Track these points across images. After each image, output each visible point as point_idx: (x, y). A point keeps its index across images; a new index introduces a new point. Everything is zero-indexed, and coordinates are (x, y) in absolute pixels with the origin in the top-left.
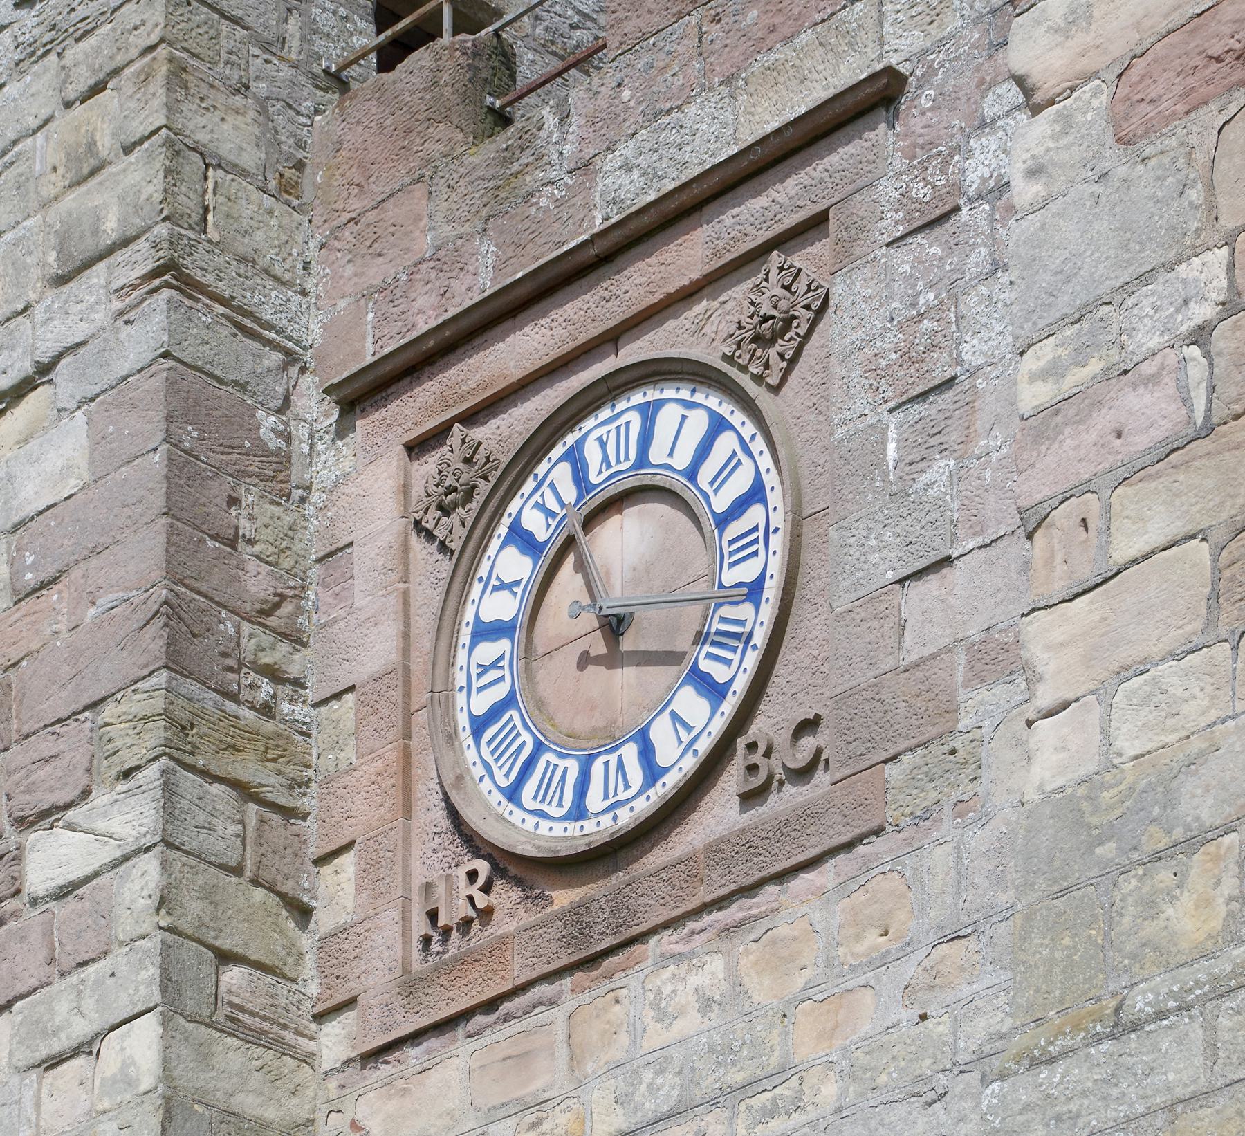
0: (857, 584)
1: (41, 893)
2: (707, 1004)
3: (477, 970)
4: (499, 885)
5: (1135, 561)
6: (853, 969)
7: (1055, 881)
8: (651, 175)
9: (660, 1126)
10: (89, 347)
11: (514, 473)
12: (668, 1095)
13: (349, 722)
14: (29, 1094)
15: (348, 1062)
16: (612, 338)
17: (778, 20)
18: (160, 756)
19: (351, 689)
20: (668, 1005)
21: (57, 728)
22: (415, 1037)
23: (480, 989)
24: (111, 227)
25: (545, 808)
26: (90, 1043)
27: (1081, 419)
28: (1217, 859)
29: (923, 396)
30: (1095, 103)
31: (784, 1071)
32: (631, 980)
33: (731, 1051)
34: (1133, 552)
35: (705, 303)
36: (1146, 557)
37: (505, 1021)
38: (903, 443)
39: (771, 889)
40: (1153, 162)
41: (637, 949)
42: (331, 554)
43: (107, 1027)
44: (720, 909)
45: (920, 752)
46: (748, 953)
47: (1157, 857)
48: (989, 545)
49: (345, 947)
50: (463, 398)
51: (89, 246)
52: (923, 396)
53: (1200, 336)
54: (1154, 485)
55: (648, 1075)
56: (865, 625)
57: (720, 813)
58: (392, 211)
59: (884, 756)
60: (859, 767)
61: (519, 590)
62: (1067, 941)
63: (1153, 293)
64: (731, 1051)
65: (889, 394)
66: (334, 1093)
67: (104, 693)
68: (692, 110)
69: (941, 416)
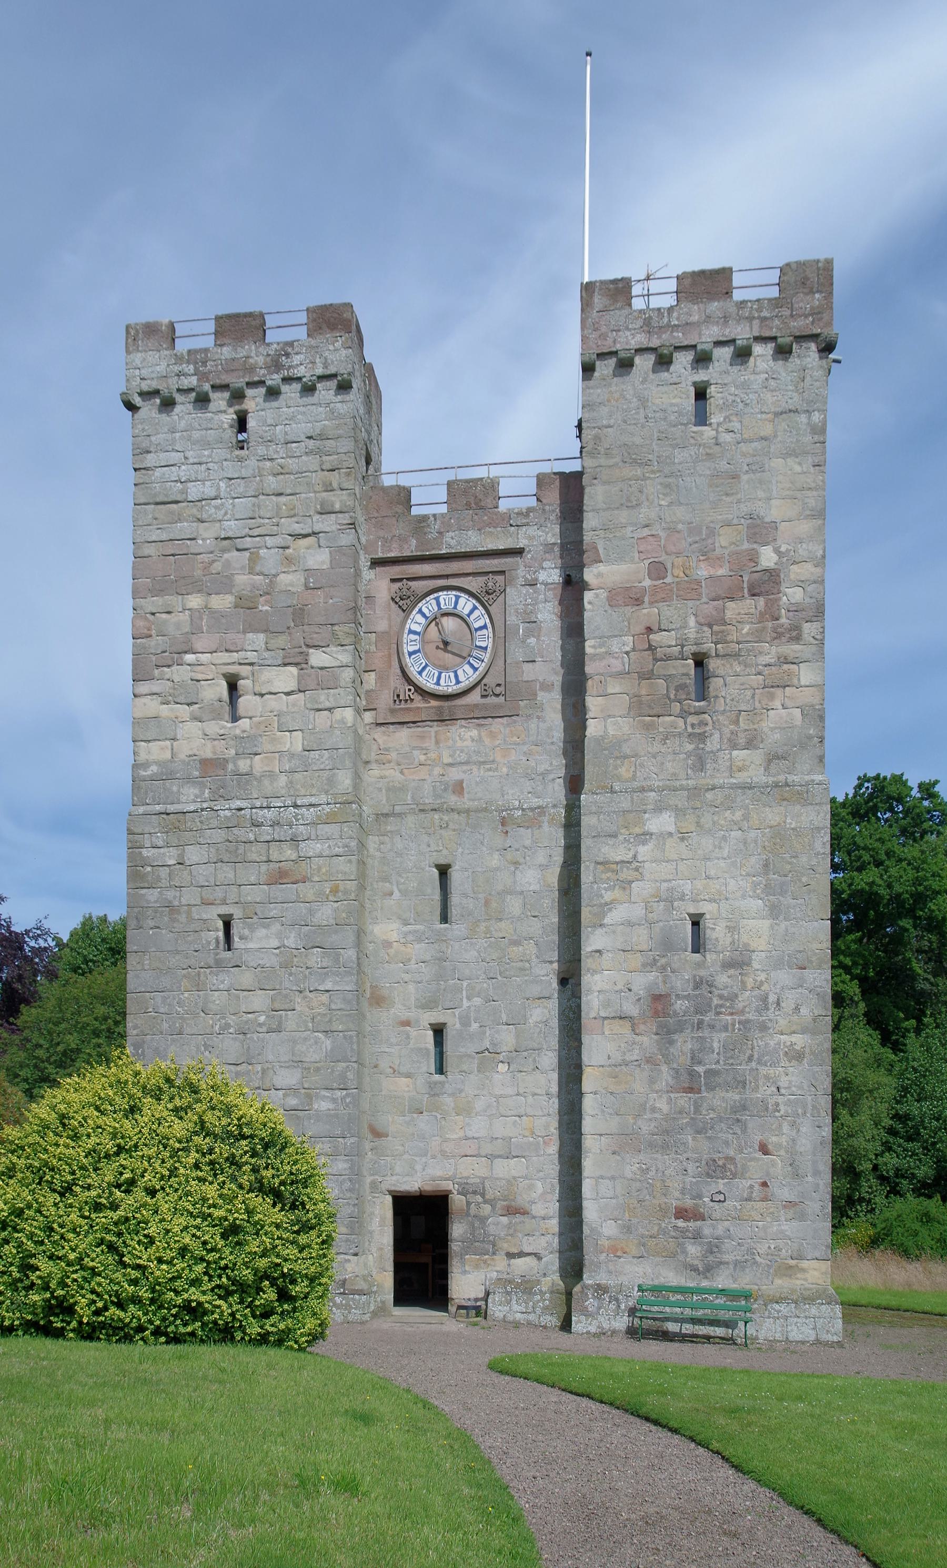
1: (315, 666)
3: (412, 713)
8: (459, 543)
13: (374, 640)
14: (311, 717)
16: (447, 577)
22: (393, 724)
24: (337, 507)
27: (601, 660)
32: (453, 728)
47: (617, 758)
51: (330, 509)
53: (627, 653)
55: (458, 752)
57: (475, 697)
58: (386, 520)
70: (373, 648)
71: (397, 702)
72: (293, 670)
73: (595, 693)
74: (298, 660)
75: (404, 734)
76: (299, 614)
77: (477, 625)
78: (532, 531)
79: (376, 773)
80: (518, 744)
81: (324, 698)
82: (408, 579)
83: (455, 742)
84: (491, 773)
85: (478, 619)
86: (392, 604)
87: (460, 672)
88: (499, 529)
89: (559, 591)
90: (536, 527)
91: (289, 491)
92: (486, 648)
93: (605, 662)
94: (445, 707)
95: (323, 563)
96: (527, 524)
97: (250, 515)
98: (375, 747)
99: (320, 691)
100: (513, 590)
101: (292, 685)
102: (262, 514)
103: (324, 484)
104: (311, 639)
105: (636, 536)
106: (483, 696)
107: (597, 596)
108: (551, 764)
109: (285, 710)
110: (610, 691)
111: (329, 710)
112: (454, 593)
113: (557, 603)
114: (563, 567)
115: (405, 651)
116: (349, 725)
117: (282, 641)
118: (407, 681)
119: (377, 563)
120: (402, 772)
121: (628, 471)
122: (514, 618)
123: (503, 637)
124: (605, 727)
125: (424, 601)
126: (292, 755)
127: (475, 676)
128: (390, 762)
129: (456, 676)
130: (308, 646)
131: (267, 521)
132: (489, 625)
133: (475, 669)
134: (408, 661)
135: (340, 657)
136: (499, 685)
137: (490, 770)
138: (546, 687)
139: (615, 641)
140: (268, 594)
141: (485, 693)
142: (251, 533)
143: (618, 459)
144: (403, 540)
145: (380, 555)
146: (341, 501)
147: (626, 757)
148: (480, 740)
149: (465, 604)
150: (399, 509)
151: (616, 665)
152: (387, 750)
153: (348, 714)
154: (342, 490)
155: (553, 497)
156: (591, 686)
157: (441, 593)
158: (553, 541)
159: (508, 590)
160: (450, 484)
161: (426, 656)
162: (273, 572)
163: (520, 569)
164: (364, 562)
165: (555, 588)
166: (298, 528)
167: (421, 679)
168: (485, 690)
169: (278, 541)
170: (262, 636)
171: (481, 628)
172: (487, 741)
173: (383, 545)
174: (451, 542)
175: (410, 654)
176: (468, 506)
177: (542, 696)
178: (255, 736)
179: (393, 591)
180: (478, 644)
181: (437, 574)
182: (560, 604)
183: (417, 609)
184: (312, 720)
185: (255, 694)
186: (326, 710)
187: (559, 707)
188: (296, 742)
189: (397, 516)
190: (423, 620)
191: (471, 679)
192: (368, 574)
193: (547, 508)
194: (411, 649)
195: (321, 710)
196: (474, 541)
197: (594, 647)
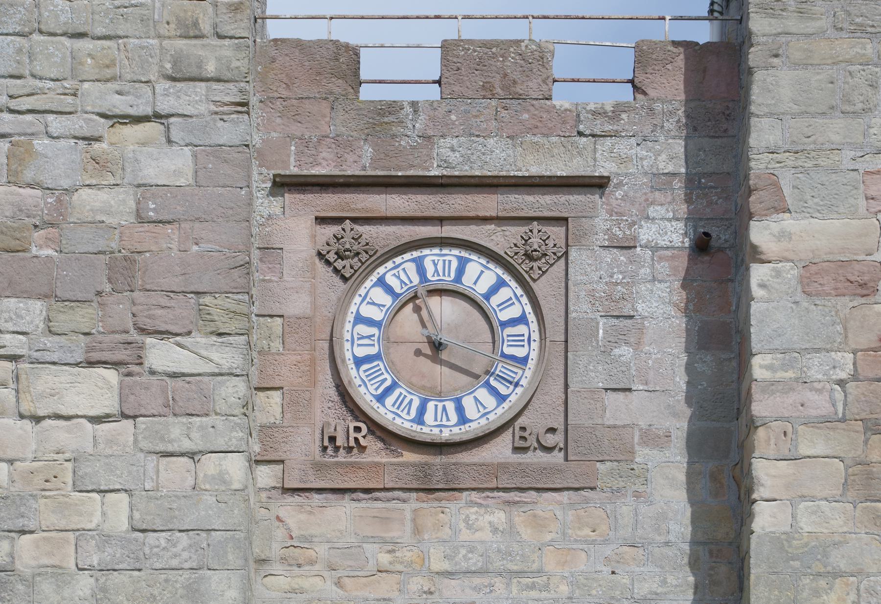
0: (582, 381)
1: (160, 369)
2: (495, 530)
3: (361, 473)
4: (370, 437)
5: (809, 457)
6: (576, 541)
7: (770, 567)
8: (467, 160)
9: (468, 575)
10: (190, 120)
12: (475, 564)
15: (274, 488)
16: (441, 220)
17: (539, 124)
20: (473, 524)
21: (172, 295)
22: (320, 491)
24: (211, 69)
25: (399, 412)
26: (194, 453)
28: (847, 585)
29: (618, 317)
30: (792, 272)
31: (540, 572)
32: (452, 507)
33: (510, 555)
34: (809, 453)
35: (493, 226)
36: (814, 457)
38: (605, 332)
39: (533, 493)
40: (820, 307)
41: (457, 494)
42: (267, 248)
45: (616, 463)
46: (519, 516)
47: (819, 574)
49: (276, 435)
50: (353, 210)
51: (194, 72)
52: (618, 317)
53: (841, 383)
54: (819, 431)
55: (463, 551)
56: (586, 401)
57: (500, 450)
58: (307, 105)
59: (597, 459)
60: (583, 458)
61: (385, 310)
62: (776, 593)
63: (819, 358)
64: (510, 555)
65: (600, 309)
66: (264, 499)
67: (205, 290)
68: (491, 141)
69: (625, 329)
70: (277, 345)
71: (330, 451)
72: (111, 376)
73: (772, 453)
74: (121, 355)
75: (344, 511)
76: (124, 269)
77: (504, 316)
78: (624, 147)
79: (282, 582)
80: (593, 542)
81: (178, 433)
82: (354, 220)
83: (456, 532)
84: (534, 594)
85: (507, 304)
86: (320, 265)
87: (468, 402)
88: (554, 139)
89: (683, 262)
90: (633, 141)
91: (100, 31)
92: (524, 361)
93: (792, 398)
94: (436, 465)
95: (177, 173)
96: (615, 135)
97: (11, 71)
98: (280, 533)
99: (171, 419)
100: (585, 254)
101: (108, 404)
102: (38, 70)
103: (181, 23)
104: (149, 317)
105: (862, 166)
106: (517, 450)
107: (778, 274)
108: (664, 582)
109: (90, 450)
110: (804, 450)
111: (191, 455)
112: (456, 252)
113: (677, 284)
114: (692, 219)
115: (348, 355)
116: (236, 486)
117: (83, 317)
118: (352, 412)
119: (283, 185)
120: (338, 583)
121: (846, 47)
122: (585, 307)
123: (561, 344)
124: (794, 516)
125: (389, 264)
126: (106, 539)
127: (500, 411)
128: (312, 563)
129: (460, 409)
130: (143, 331)
131: (51, 84)
132: (531, 317)
133: (502, 398)
134: (353, 375)
135: (215, 356)
136: (552, 430)
137: (533, 587)
138: (654, 439)
139: (816, 359)
140: (52, 225)
141: (522, 444)
142: (13, 104)
143: (824, 23)
144: (343, 144)
145: (294, 170)
146: (219, 59)
147: (837, 574)
148: (511, 530)
149: (480, 276)
150: (338, 86)
151: (819, 404)
152: (308, 539)
153: (235, 467)
154: (220, 37)
155: (671, 87)
156: (763, 440)
157: (426, 252)
158: (670, 168)
159: (573, 254)
160: (447, 47)
161: (392, 367)
162: (65, 183)
163: (598, 216)
164: (261, 182)
165: (673, 257)
166: (120, 105)
167: (382, 410)
168: (523, 438)
169: (77, 124)
170: (37, 306)
171: (513, 322)
172: (526, 533)
173: (300, 153)
174: (450, 156)
175: (359, 362)
176: (488, 92)
177: (643, 455)
178: (22, 498)
179: (321, 240)
180: (508, 351)
181: (419, 214)
182: (684, 286)
183: (374, 278)
184: (151, 472)
185: (22, 417)
186: (182, 455)
187: (682, 477)
188: (118, 513)
189: (332, 100)
190: (387, 300)
191: (492, 417)
192: (268, 206)
193: (658, 107)
194: (361, 352)
195: (171, 455)
196: (499, 157)
197: (770, 368)
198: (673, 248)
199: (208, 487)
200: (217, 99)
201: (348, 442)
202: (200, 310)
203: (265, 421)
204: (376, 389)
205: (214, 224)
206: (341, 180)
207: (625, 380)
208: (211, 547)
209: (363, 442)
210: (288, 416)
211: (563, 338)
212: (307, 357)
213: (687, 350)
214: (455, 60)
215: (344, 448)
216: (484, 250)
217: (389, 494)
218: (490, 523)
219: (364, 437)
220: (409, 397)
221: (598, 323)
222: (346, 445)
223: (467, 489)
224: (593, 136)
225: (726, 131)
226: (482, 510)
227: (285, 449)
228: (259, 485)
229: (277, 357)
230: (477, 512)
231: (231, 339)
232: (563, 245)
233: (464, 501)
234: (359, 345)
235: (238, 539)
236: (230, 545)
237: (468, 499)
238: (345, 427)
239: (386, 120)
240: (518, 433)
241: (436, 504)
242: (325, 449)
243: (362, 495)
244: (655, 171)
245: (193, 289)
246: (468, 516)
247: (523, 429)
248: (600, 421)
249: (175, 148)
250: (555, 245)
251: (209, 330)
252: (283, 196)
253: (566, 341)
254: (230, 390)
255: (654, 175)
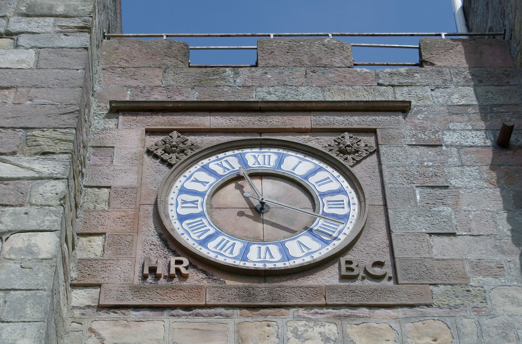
3: (182, 294)
11: (209, 152)
15: (89, 307)
17: (343, 80)
18: (69, 153)
19: (109, 187)
23: (183, 300)
29: (433, 187)
37: (196, 315)
41: (283, 311)
42: (100, 147)
43: (19, 230)
44: (333, 309)
48: (475, 236)
52: (433, 187)
56: (411, 242)
57: (329, 277)
70: (103, 206)
71: (150, 279)
86: (148, 160)
89: (488, 155)
106: (343, 278)
113: (486, 168)
119: (118, 109)
136: (379, 264)
159: (383, 149)
164: (98, 108)
165: (477, 152)
175: (182, 218)
198: (477, 146)
199: (13, 256)
200: (63, 24)
201: (169, 271)
202: (27, 139)
203: (85, 256)
204: (199, 236)
205: (49, 89)
206: (171, 105)
207: (448, 228)
208: (8, 303)
209: (184, 271)
210: (108, 253)
211: (381, 203)
212: (131, 212)
213: (505, 209)
214: (270, 48)
215: (165, 277)
216: (300, 147)
217: (212, 311)
218: (320, 333)
219: (187, 268)
220: (232, 242)
221: (414, 191)
222: (167, 274)
223: (293, 306)
224: (393, 86)
225: (508, 82)
226: (312, 324)
227: (104, 276)
228: (73, 304)
229: (102, 213)
230: (306, 325)
231: (55, 156)
232: (374, 145)
233: (291, 316)
234: (182, 207)
235: (40, 297)
236: (30, 301)
237: (296, 314)
238: (165, 262)
239: (210, 78)
240: (344, 266)
241: (261, 319)
242: (144, 277)
243: (181, 312)
244: (450, 103)
245: (22, 125)
246: (296, 328)
247: (349, 262)
248: (428, 256)
249: (20, 50)
250: (366, 146)
251: (33, 152)
252: (118, 118)
253: (385, 205)
254: (48, 188)
255: (450, 106)
